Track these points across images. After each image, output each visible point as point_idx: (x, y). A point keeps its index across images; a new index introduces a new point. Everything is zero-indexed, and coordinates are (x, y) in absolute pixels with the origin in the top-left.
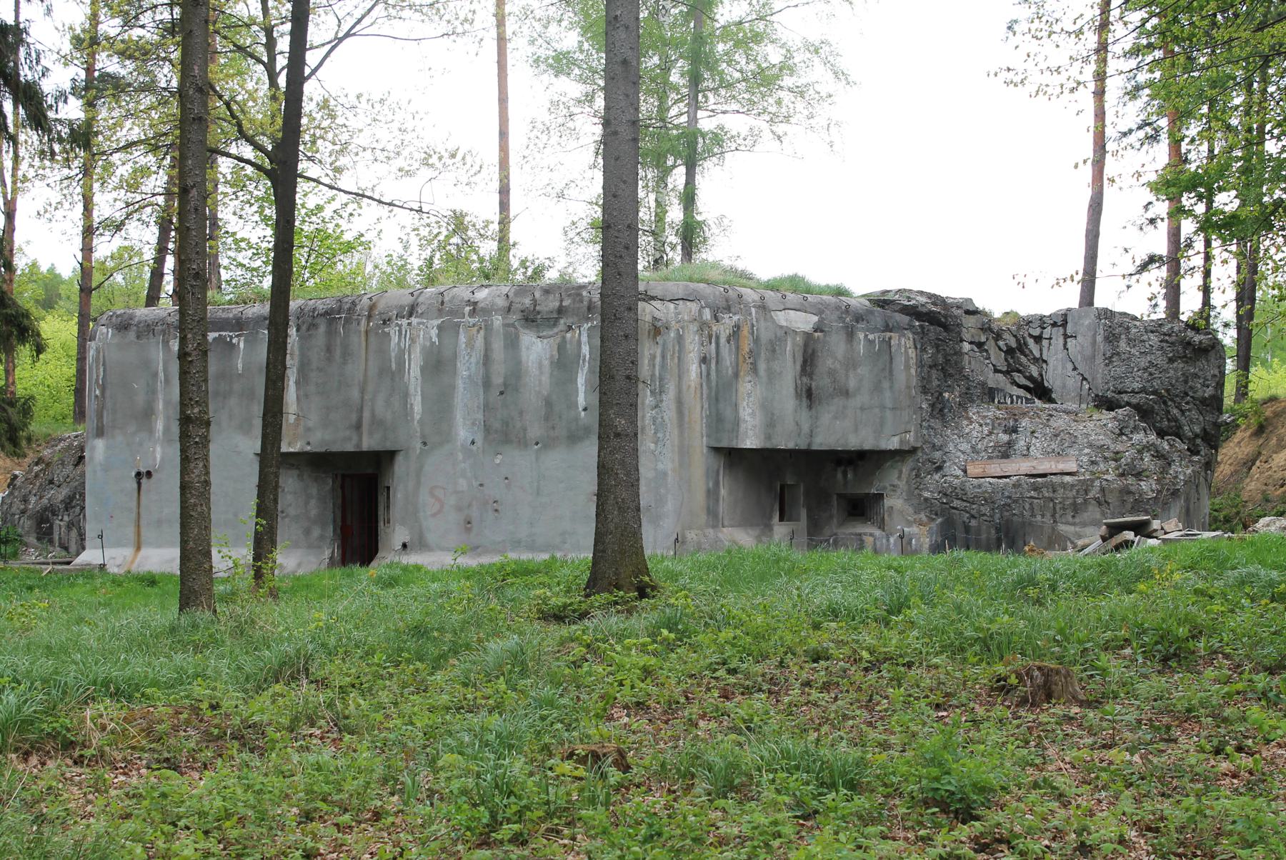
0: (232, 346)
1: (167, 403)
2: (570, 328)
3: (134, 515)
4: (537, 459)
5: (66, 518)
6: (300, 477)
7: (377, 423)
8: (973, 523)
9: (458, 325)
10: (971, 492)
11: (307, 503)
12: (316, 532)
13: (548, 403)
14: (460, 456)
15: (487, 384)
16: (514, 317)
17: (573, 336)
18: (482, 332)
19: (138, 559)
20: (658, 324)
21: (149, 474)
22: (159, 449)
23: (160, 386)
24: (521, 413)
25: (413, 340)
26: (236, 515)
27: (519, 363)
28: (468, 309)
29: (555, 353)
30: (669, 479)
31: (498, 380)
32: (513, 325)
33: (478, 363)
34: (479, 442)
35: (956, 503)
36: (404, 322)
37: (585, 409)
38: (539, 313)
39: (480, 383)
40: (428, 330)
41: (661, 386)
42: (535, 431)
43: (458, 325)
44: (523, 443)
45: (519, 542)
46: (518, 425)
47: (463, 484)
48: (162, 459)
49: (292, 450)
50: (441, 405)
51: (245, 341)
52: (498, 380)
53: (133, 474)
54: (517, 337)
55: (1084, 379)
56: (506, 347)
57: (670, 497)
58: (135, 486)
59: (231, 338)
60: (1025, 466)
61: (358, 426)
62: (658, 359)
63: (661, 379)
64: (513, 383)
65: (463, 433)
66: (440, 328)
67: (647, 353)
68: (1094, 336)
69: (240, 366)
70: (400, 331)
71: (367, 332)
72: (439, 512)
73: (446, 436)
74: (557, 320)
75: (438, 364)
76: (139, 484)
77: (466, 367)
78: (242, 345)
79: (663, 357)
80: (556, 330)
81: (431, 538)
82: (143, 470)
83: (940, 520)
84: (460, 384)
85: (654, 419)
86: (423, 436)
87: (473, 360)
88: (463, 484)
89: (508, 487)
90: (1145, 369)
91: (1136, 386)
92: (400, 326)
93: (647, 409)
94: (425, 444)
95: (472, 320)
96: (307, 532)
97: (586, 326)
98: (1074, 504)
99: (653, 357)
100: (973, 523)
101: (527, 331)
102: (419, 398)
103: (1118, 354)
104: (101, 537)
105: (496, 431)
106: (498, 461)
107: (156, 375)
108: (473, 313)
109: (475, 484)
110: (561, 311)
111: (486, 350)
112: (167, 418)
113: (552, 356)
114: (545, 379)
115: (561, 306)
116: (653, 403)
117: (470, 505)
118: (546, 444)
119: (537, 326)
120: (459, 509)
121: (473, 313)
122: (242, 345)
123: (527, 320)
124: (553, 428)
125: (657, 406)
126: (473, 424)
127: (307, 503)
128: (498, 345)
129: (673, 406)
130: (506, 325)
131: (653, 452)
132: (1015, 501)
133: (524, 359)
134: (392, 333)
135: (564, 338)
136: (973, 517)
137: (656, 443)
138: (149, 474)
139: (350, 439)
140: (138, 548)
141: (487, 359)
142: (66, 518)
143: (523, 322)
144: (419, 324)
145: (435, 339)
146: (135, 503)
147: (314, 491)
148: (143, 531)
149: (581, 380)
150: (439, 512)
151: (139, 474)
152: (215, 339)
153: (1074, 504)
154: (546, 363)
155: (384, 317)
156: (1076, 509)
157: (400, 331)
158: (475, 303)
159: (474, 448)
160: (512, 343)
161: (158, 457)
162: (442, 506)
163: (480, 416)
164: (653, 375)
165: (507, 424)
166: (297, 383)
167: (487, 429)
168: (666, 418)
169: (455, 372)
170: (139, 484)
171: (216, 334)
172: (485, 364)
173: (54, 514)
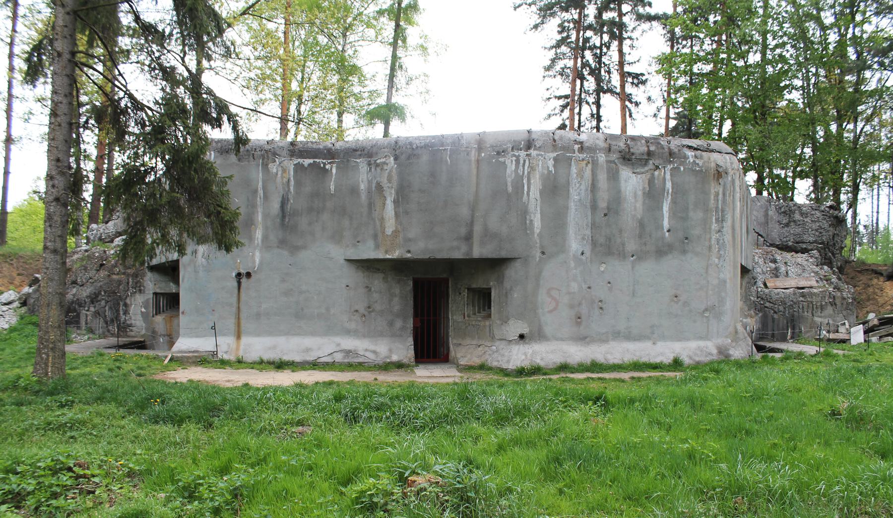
0: (325, 171)
1: (266, 216)
2: (657, 168)
3: (234, 309)
4: (633, 268)
5: (92, 309)
6: (385, 279)
7: (487, 235)
8: (776, 316)
9: (570, 159)
10: (775, 297)
11: (390, 300)
12: (399, 324)
13: (641, 224)
14: (572, 264)
15: (594, 207)
16: (614, 156)
17: (660, 174)
18: (590, 166)
19: (242, 347)
20: (720, 170)
21: (248, 275)
22: (258, 254)
23: (259, 201)
24: (621, 231)
25: (532, 168)
26: (328, 309)
27: (619, 192)
28: (576, 147)
29: (647, 186)
30: (728, 285)
31: (603, 204)
32: (614, 162)
33: (587, 190)
34: (588, 253)
35: (767, 304)
36: (523, 154)
37: (669, 231)
38: (633, 154)
39: (589, 206)
40: (546, 161)
41: (723, 216)
42: (631, 246)
43: (570, 159)
44: (622, 255)
45: (619, 333)
46: (619, 240)
47: (574, 286)
48: (261, 263)
49: (388, 257)
50: (556, 222)
51: (337, 168)
52: (603, 204)
53: (234, 274)
54: (617, 171)
55: (759, 235)
56: (609, 179)
57: (728, 299)
58: (236, 284)
59: (324, 164)
60: (792, 282)
61: (468, 238)
62: (721, 196)
63: (723, 211)
64: (614, 209)
65: (575, 245)
66: (555, 159)
67: (713, 191)
68: (767, 210)
69: (332, 187)
70: (518, 161)
71: (478, 161)
72: (555, 309)
73: (562, 247)
74: (647, 161)
75: (554, 189)
76: (239, 283)
77: (577, 192)
78: (334, 171)
79: (724, 194)
80: (646, 168)
81: (548, 330)
82: (243, 271)
83: (760, 315)
84: (572, 205)
85: (718, 241)
86: (542, 247)
87: (583, 187)
88: (574, 286)
89: (610, 289)
90: (817, 230)
91: (811, 239)
92: (518, 157)
93: (713, 233)
94: (543, 253)
95: (581, 156)
96: (391, 324)
97: (669, 167)
98: (821, 305)
99: (717, 194)
100: (776, 316)
101: (625, 168)
102: (538, 216)
103: (794, 221)
104: (213, 328)
105: (601, 245)
106: (602, 269)
107: (255, 191)
108: (582, 150)
109: (585, 286)
110: (649, 154)
111: (593, 180)
112: (266, 228)
113: (644, 188)
114: (639, 205)
115: (649, 150)
116: (717, 229)
117: (580, 304)
118: (640, 256)
119: (633, 164)
120: (571, 307)
121: (582, 150)
122: (334, 171)
123: (624, 159)
124: (645, 244)
125: (719, 231)
126: (583, 239)
127: (390, 300)
128: (602, 177)
129: (730, 232)
130: (608, 162)
131: (717, 265)
132: (795, 303)
133: (623, 189)
134: (508, 162)
135: (653, 174)
136: (775, 312)
137: (719, 259)
138: (248, 275)
139: (458, 248)
140: (239, 337)
141: (594, 187)
142: (92, 309)
143: (621, 160)
144: (538, 155)
145: (552, 168)
146: (235, 299)
147: (397, 291)
148: (243, 322)
149: (666, 208)
150: (555, 309)
151: (239, 275)
152: (310, 165)
153: (821, 305)
154: (640, 193)
155: (497, 149)
156: (822, 308)
157: (518, 161)
158: (581, 143)
159: (583, 257)
160: (614, 176)
161: (257, 261)
162: (557, 305)
163: (588, 232)
164: (717, 208)
165: (610, 239)
166: (396, 202)
167: (594, 243)
168: (726, 240)
169: (568, 196)
170: (239, 283)
171: (311, 161)
172: (592, 191)
173: (80, 306)
